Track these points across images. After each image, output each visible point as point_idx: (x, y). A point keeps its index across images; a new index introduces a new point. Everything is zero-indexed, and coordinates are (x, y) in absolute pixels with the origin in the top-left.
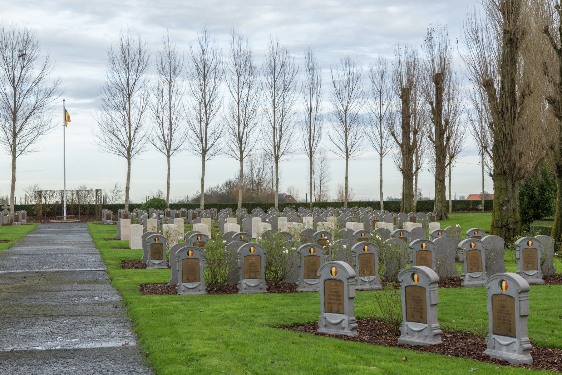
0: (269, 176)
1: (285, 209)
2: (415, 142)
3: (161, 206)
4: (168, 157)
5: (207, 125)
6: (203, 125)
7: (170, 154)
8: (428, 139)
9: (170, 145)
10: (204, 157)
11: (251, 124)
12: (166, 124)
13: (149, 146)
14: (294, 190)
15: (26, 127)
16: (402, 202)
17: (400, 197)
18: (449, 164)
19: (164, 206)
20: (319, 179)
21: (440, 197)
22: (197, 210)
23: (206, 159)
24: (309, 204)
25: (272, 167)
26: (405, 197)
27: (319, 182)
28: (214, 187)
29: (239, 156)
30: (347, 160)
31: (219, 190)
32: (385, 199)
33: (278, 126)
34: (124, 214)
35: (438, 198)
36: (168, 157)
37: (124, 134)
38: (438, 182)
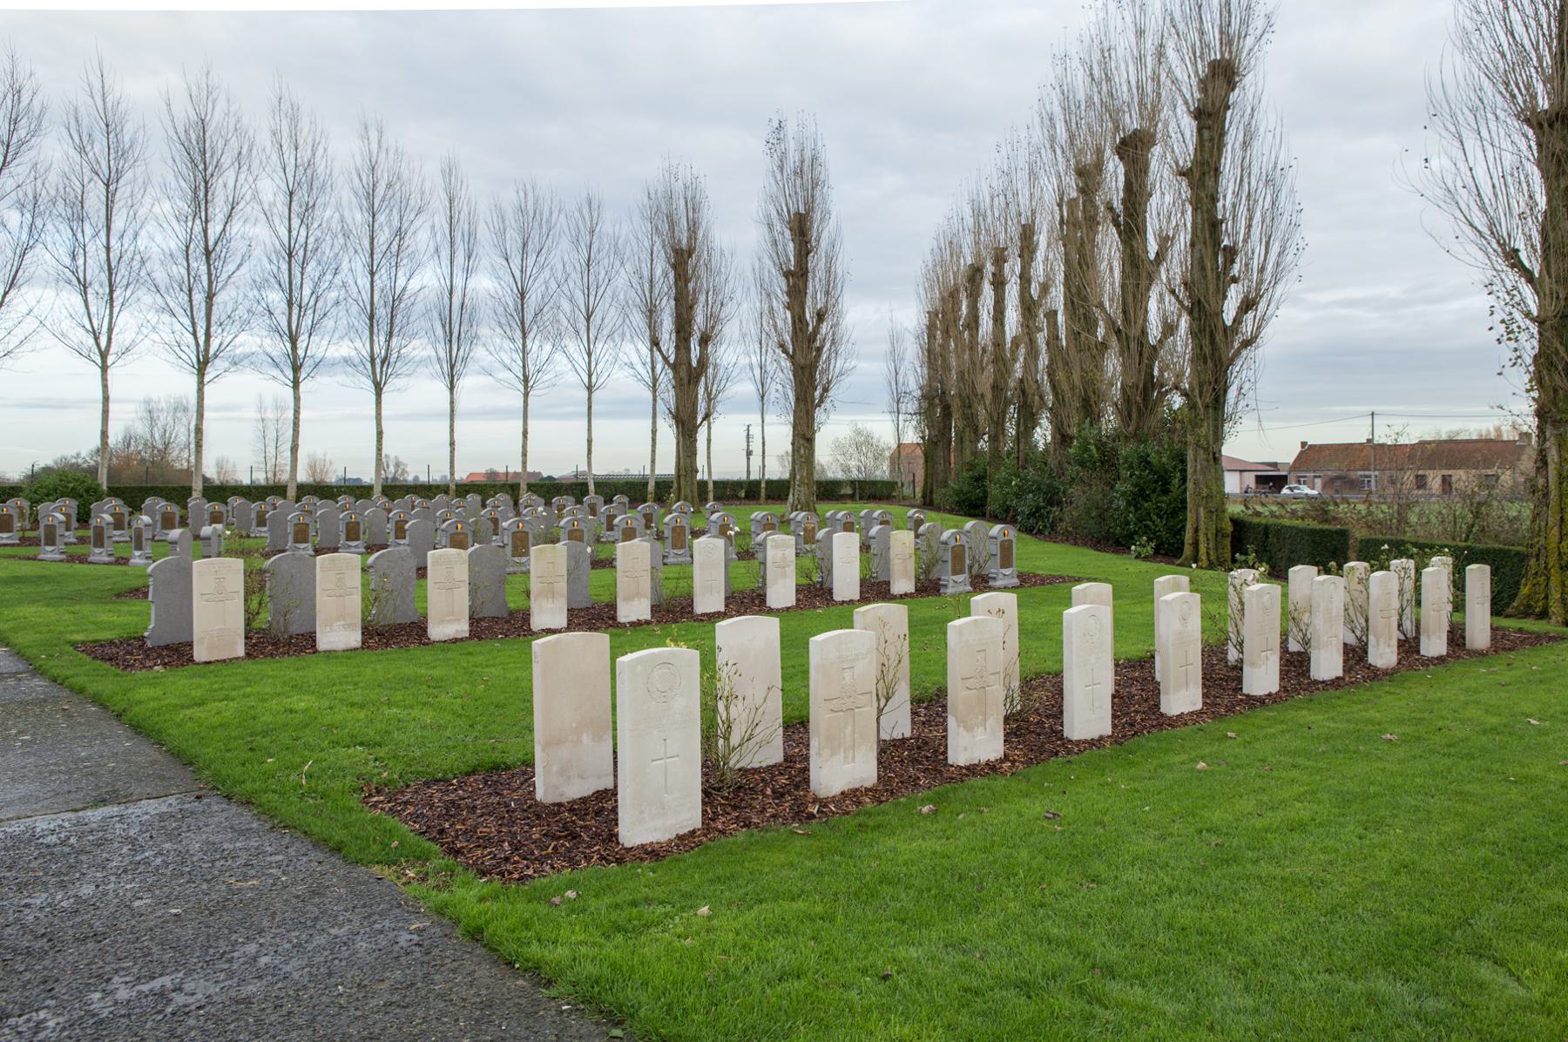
0: (182, 438)
1: (148, 501)
2: (703, 363)
3: (87, 491)
4: (104, 368)
5: (210, 297)
6: (199, 297)
7: (109, 363)
8: (779, 351)
9: (109, 339)
10: (201, 373)
13: (45, 339)
14: (227, 462)
16: (675, 485)
17: (673, 472)
18: (707, 416)
19: (96, 491)
20: (274, 446)
21: (805, 474)
22: (13, 505)
23: (206, 379)
24: (757, 483)
25: (189, 424)
26: (682, 472)
27: (273, 452)
28: (72, 457)
29: (291, 377)
30: (526, 395)
31: (80, 461)
32: (715, 477)
34: (163, 514)
35: (802, 476)
36: (104, 368)
38: (802, 442)
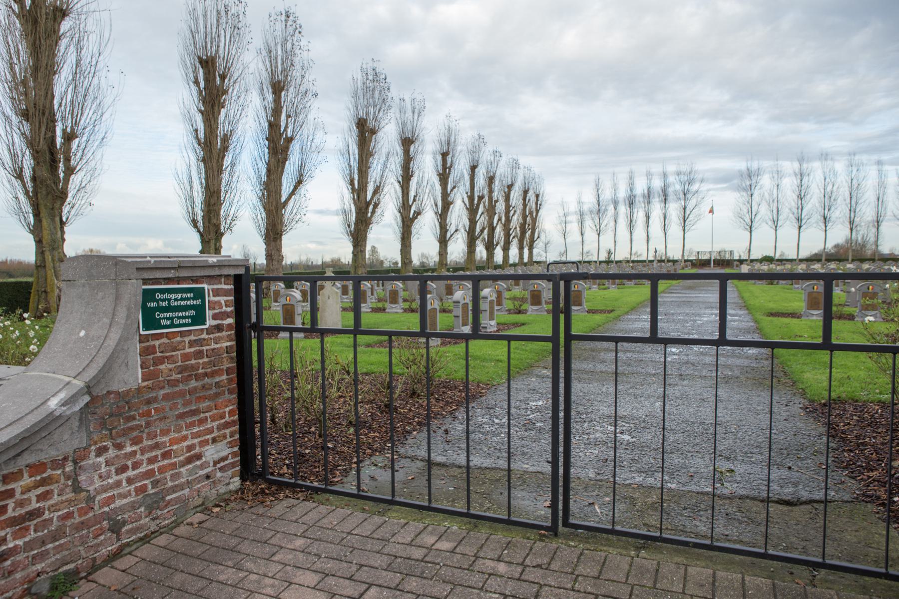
6: (800, 210)
11: (833, 209)
12: (775, 211)
15: (691, 216)
33: (852, 209)
37: (748, 218)
